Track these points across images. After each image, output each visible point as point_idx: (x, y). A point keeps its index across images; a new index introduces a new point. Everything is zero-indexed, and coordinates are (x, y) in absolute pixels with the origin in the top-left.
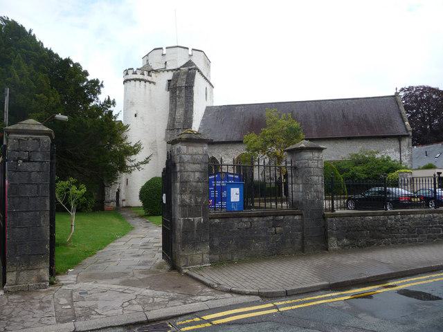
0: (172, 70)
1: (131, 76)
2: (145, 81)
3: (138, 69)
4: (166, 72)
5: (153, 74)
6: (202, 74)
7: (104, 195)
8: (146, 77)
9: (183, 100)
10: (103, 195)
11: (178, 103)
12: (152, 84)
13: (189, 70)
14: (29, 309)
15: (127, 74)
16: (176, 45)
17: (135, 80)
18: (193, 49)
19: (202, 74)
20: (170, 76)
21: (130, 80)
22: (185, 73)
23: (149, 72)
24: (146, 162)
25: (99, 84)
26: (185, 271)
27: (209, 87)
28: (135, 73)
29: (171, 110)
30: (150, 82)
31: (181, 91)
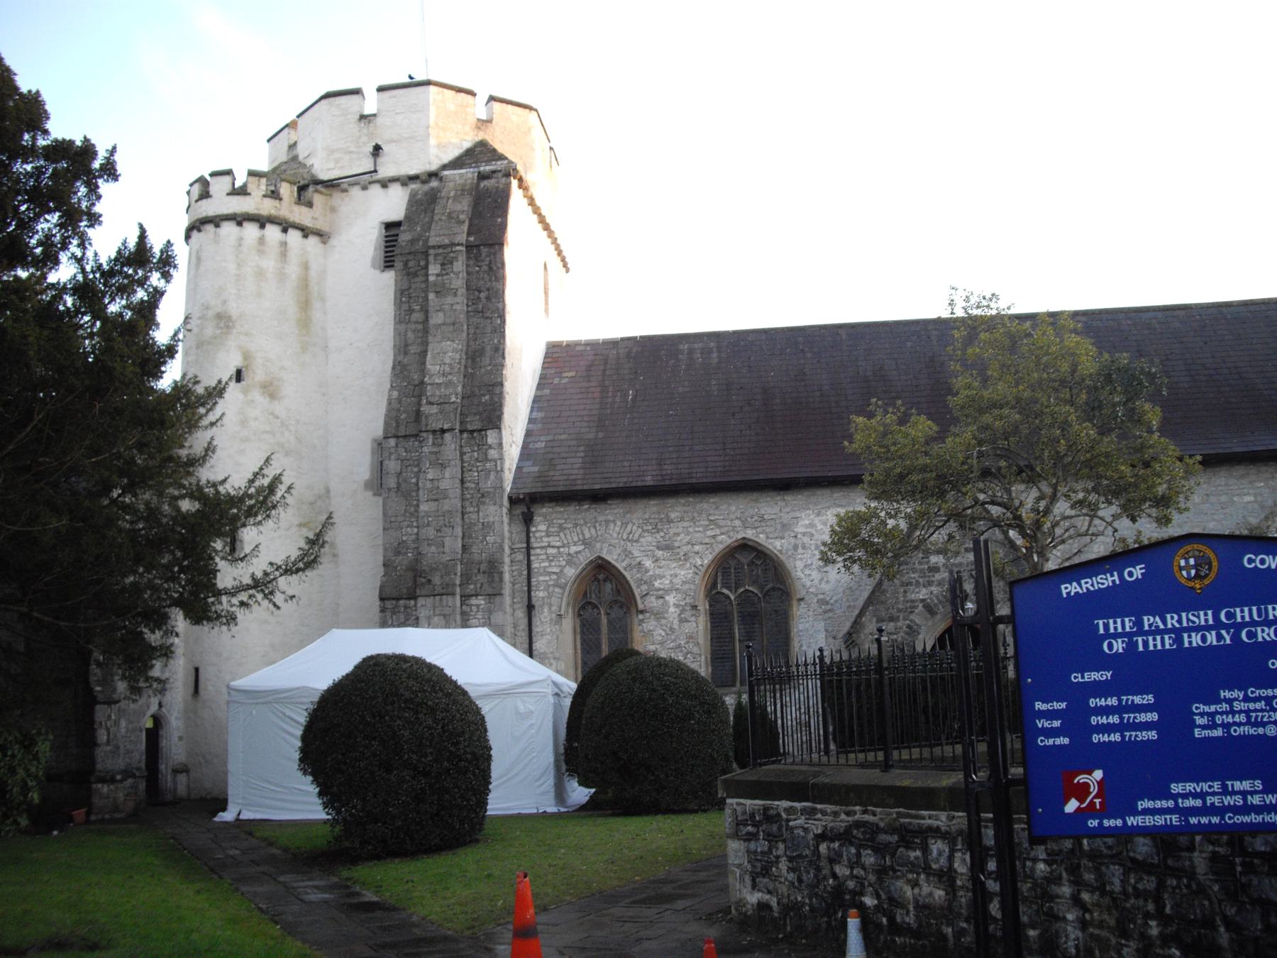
1: (221, 203)
2: (286, 226)
3: (252, 174)
4: (376, 190)
5: (318, 199)
7: (94, 744)
8: (288, 208)
9: (459, 302)
10: (88, 741)
11: (436, 319)
12: (313, 240)
13: (482, 177)
14: (592, 379)
16: (322, 93)
17: (240, 219)
18: (492, 99)
20: (393, 204)
21: (216, 221)
22: (462, 191)
23: (302, 189)
24: (306, 561)
25: (96, 165)
27: (555, 262)
28: (242, 191)
29: (402, 348)
30: (306, 232)
31: (446, 264)
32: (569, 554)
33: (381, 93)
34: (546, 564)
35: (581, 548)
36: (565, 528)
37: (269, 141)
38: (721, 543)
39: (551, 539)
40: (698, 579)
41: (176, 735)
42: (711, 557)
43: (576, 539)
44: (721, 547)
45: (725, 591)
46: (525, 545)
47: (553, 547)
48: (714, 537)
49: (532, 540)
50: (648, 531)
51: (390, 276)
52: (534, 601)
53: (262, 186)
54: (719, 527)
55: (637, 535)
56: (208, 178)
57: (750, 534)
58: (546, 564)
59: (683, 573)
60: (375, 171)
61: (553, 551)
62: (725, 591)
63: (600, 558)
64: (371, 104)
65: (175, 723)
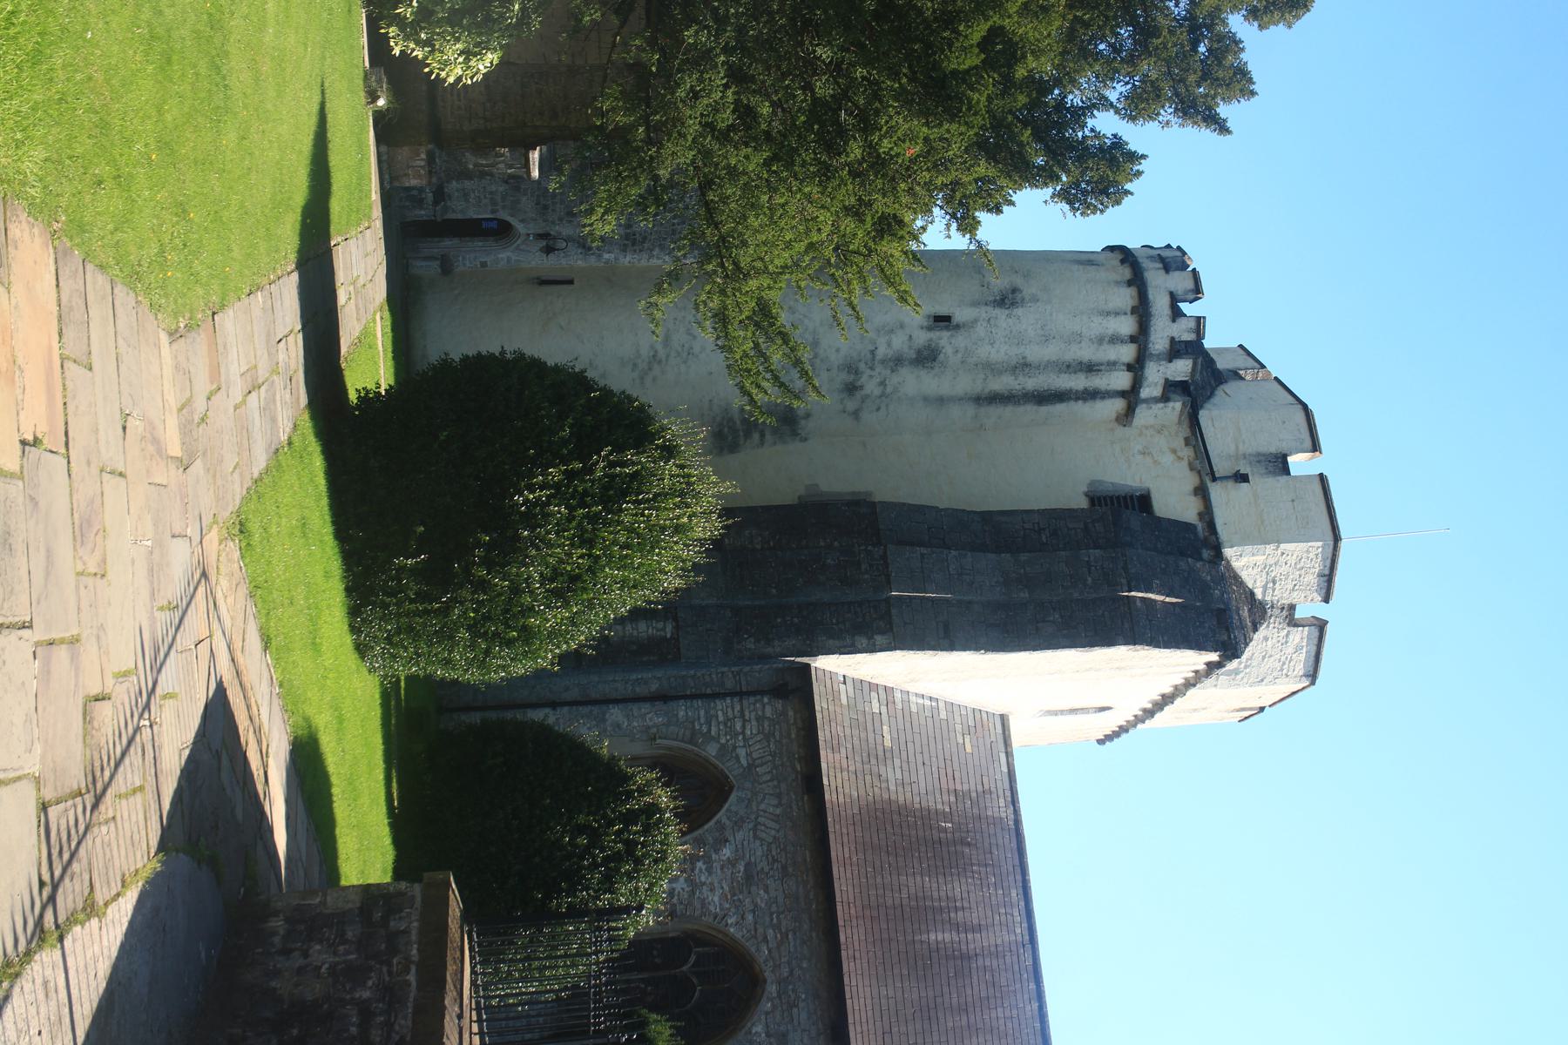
0: (1207, 515)
1: (1160, 285)
2: (1136, 368)
3: (1200, 321)
4: (1191, 481)
5: (1177, 405)
6: (1189, 684)
8: (1156, 375)
15: (1168, 123)
19: (1189, 684)
26: (387, 979)
27: (1110, 722)
32: (735, 748)
33: (1318, 478)
34: (721, 718)
35: (744, 762)
36: (768, 742)
37: (1241, 346)
38: (758, 950)
39: (754, 723)
40: (708, 919)
41: (489, 259)
42: (739, 936)
43: (755, 755)
44: (753, 949)
45: (693, 958)
46: (744, 689)
47: (744, 727)
48: (765, 940)
49: (752, 699)
50: (770, 850)
51: (1083, 503)
52: (673, 704)
53: (1183, 331)
54: (778, 947)
55: (763, 835)
56: (1190, 269)
57: (772, 989)
58: (721, 718)
59: (716, 899)
60: (1214, 479)
61: (738, 727)
62: (693, 958)
63: (731, 789)
64: (1300, 463)
65: (502, 256)
